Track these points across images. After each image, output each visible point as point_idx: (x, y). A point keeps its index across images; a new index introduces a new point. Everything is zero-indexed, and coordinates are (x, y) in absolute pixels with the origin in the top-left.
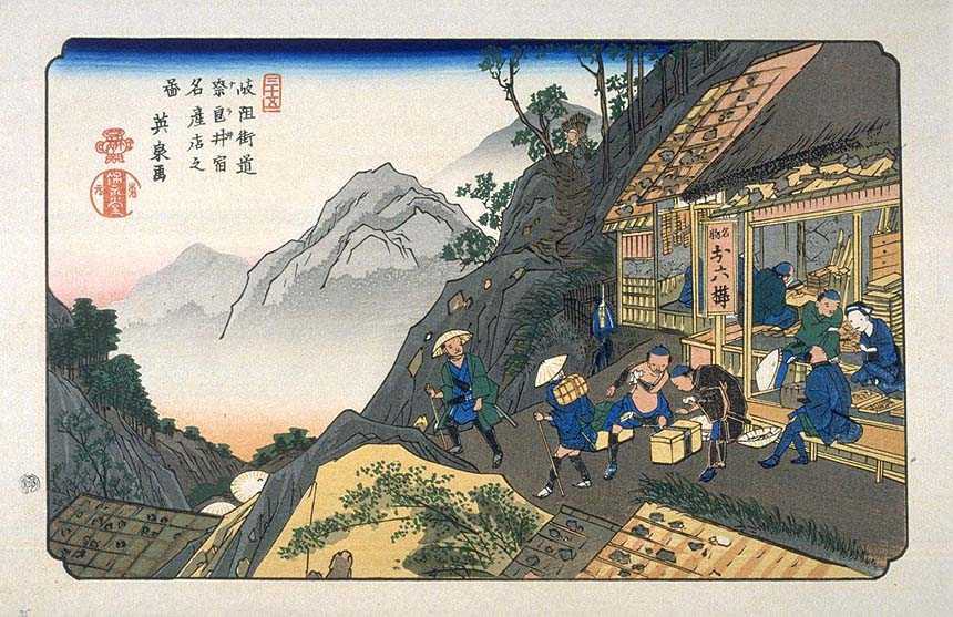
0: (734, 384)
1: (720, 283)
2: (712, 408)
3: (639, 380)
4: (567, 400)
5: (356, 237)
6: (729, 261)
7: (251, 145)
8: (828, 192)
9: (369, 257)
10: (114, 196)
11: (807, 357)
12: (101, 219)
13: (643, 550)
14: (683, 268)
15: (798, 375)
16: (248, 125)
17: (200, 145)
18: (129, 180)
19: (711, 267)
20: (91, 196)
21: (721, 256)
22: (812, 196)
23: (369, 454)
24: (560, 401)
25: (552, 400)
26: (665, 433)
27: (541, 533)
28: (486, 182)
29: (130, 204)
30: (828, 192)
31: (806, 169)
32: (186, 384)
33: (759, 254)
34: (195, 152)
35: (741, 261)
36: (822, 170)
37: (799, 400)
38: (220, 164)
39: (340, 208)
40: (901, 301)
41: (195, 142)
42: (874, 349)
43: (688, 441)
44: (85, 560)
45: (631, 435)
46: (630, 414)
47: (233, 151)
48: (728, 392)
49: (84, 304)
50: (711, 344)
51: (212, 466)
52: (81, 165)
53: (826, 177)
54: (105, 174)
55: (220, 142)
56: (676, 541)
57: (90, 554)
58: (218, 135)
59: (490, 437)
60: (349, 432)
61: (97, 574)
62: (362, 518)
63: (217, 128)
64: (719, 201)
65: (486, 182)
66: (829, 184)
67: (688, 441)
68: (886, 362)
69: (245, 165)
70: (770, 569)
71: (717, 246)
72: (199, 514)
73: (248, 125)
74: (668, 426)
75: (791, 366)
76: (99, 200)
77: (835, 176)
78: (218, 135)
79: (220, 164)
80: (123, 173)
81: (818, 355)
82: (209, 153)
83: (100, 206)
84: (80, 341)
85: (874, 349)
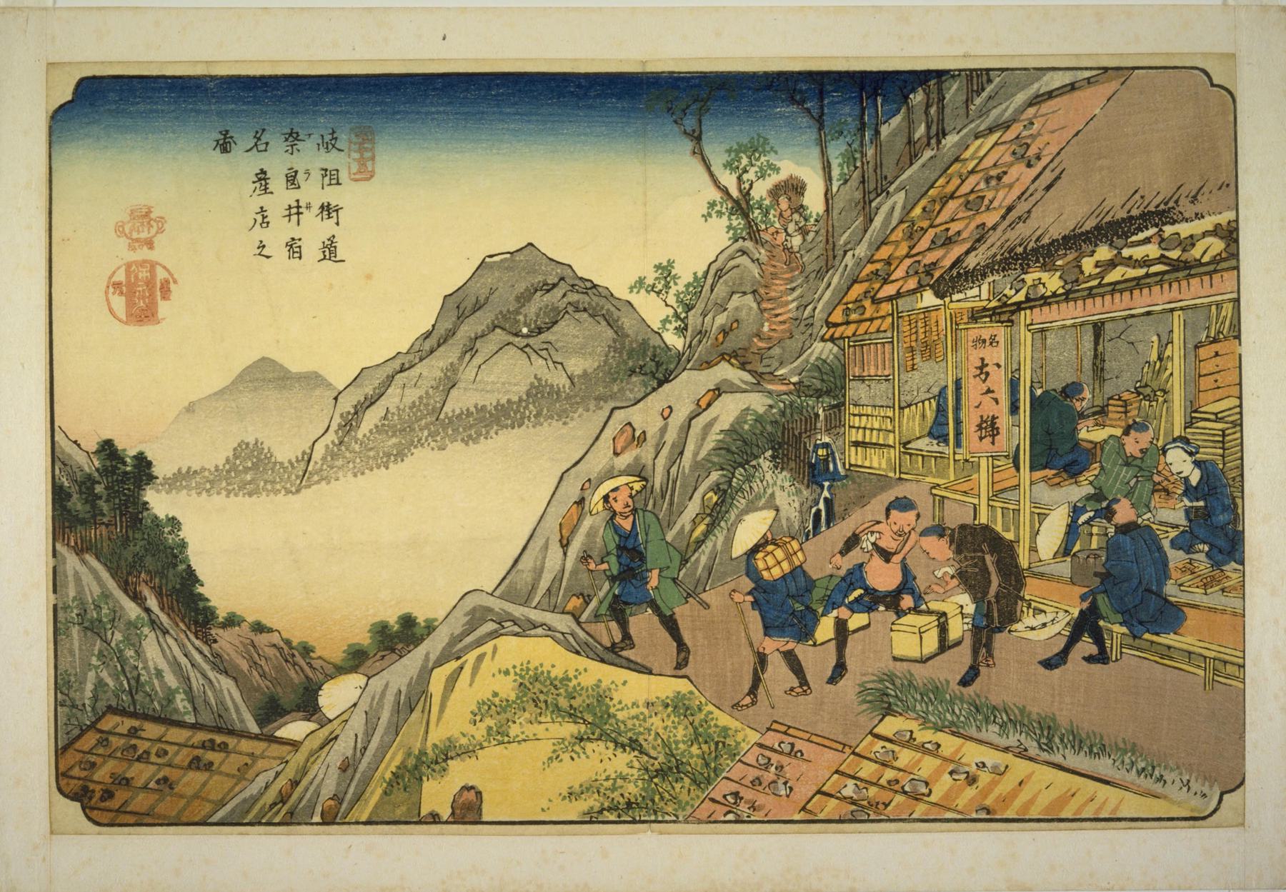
0: (1004, 550)
1: (989, 409)
2: (972, 581)
3: (874, 544)
4: (776, 572)
5: (485, 348)
6: (999, 381)
7: (337, 224)
8: (1138, 283)
9: (505, 374)
10: (142, 297)
11: (1108, 514)
12: (132, 329)
13: (883, 782)
14: (935, 390)
15: (1095, 538)
16: (332, 195)
17: (265, 223)
18: (161, 274)
19: (973, 389)
20: (107, 300)
21: (987, 374)
22: (1115, 288)
23: (514, 651)
24: (765, 574)
25: (752, 572)
26: (910, 619)
27: (744, 759)
28: (666, 272)
29: (163, 308)
30: (1138, 283)
31: (1104, 253)
32: (241, 552)
33: (1040, 366)
34: (259, 233)
35: (1014, 385)
36: (1126, 252)
37: (1096, 574)
38: (293, 247)
39: (460, 306)
40: (1238, 435)
41: (259, 218)
42: (1201, 503)
43: (943, 629)
44: (114, 804)
45: (866, 622)
46: (859, 592)
47: (313, 231)
48: (998, 563)
49: (108, 449)
50: (973, 496)
51: (289, 685)
52: (97, 254)
53: (1130, 262)
54: (129, 265)
55: (294, 218)
56: (928, 766)
57: (121, 795)
58: (290, 207)
59: (671, 625)
60: (483, 622)
61: (132, 819)
62: (500, 735)
63: (290, 197)
64: (985, 296)
65: (666, 272)
66: (1133, 273)
67: (943, 629)
68: (1217, 522)
69: (330, 250)
70: (1079, 810)
71: (983, 359)
72: (272, 739)
73: (332, 195)
74: (916, 610)
75: (1085, 529)
76: (119, 303)
77: (1146, 262)
78: (290, 207)
79: (293, 247)
80: (153, 265)
81: (1124, 512)
82: (279, 232)
83: (121, 313)
84: (103, 504)
85: (1201, 503)
